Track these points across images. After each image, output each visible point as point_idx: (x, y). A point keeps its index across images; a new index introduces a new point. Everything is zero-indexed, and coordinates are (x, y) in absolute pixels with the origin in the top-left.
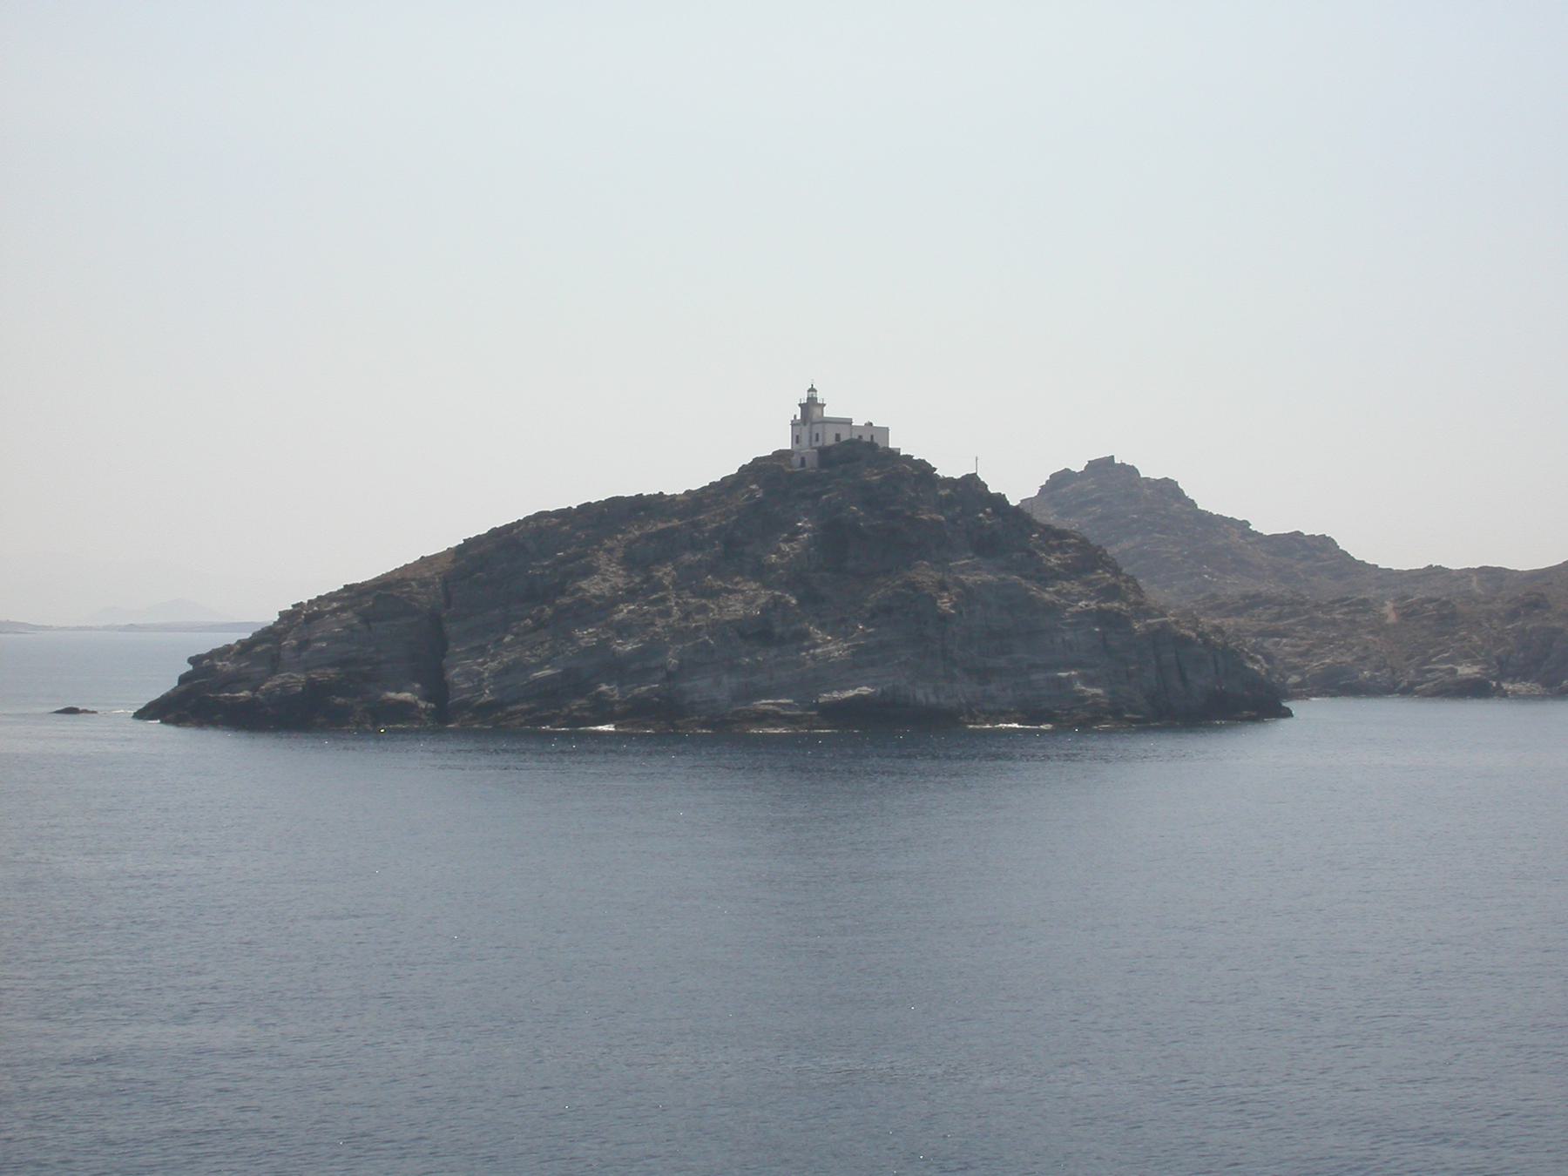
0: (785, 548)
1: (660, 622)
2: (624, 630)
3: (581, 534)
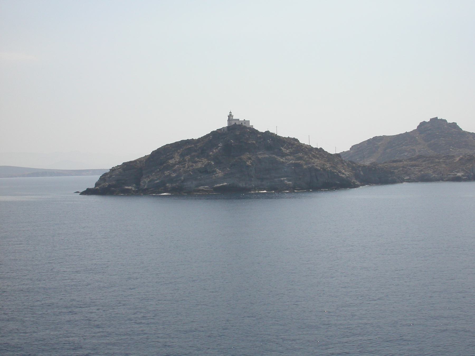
0: (214, 151)
1: (182, 169)
2: (175, 171)
3: (173, 149)
